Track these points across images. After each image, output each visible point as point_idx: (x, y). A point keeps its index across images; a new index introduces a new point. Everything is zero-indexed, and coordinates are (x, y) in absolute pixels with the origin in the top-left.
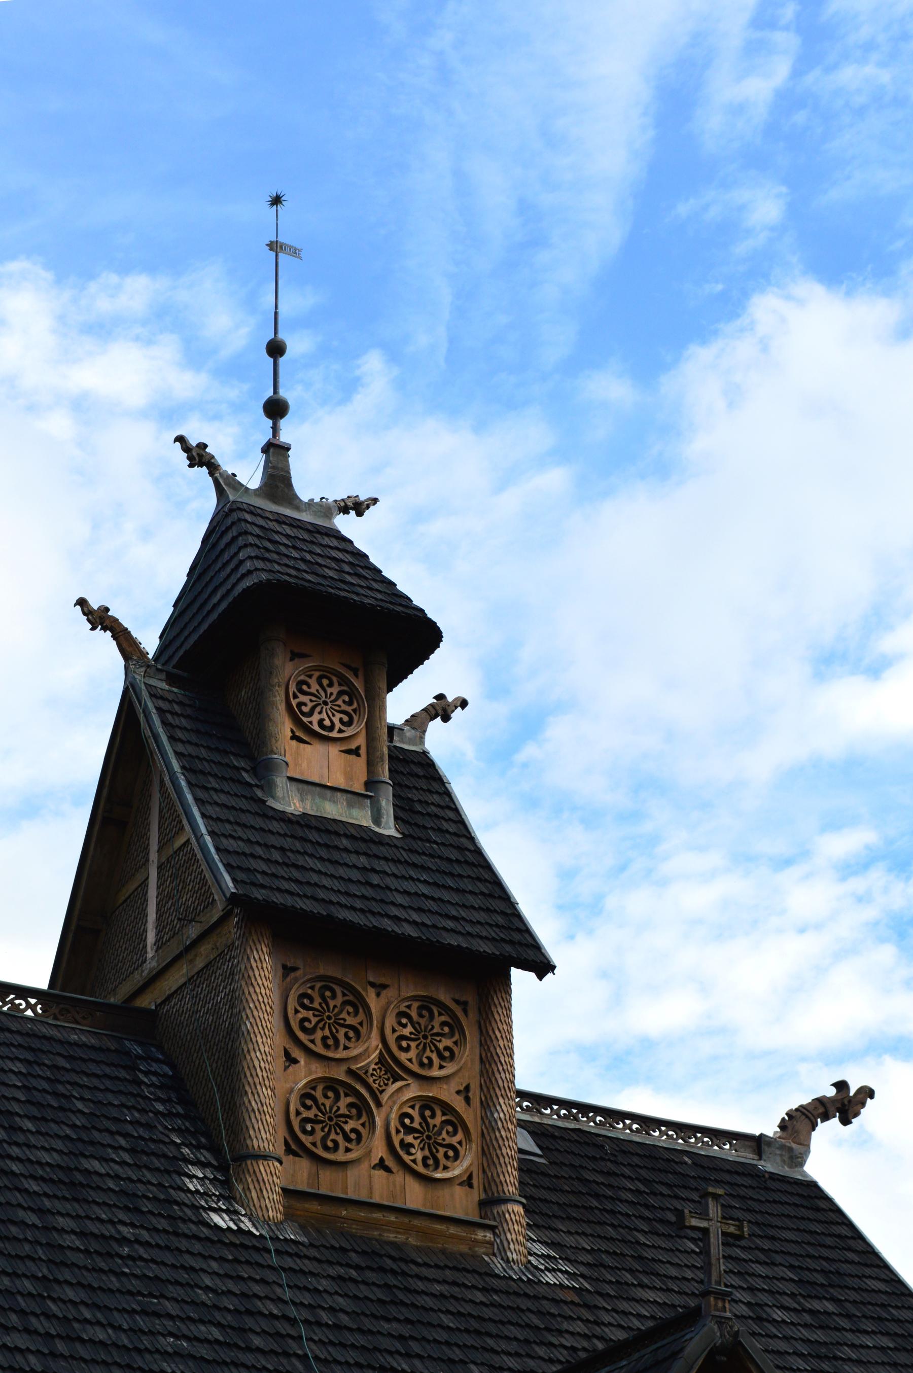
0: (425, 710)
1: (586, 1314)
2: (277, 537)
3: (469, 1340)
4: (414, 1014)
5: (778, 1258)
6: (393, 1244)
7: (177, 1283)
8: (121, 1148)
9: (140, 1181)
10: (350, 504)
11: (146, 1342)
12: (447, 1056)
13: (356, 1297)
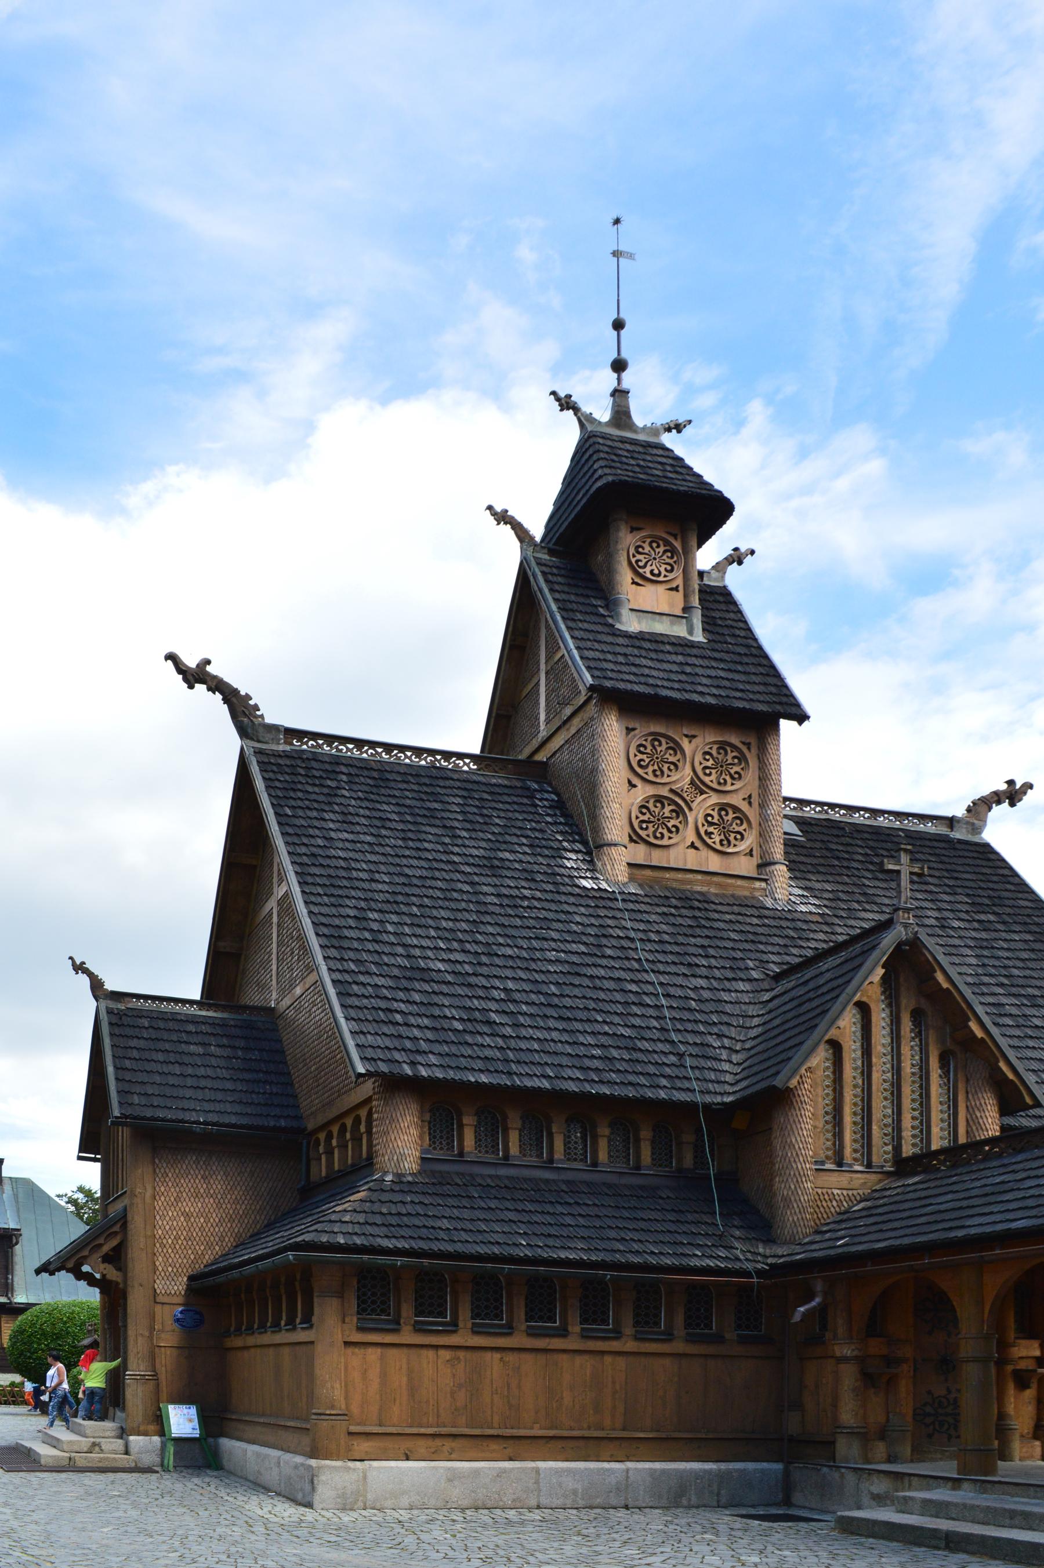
0: (726, 558)
1: (826, 928)
2: (620, 452)
3: (747, 946)
4: (714, 752)
5: (959, 890)
6: (699, 893)
7: (559, 921)
8: (524, 844)
9: (535, 863)
10: (672, 425)
11: (538, 955)
12: (737, 777)
13: (674, 924)
